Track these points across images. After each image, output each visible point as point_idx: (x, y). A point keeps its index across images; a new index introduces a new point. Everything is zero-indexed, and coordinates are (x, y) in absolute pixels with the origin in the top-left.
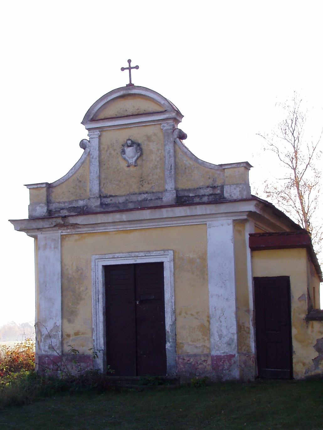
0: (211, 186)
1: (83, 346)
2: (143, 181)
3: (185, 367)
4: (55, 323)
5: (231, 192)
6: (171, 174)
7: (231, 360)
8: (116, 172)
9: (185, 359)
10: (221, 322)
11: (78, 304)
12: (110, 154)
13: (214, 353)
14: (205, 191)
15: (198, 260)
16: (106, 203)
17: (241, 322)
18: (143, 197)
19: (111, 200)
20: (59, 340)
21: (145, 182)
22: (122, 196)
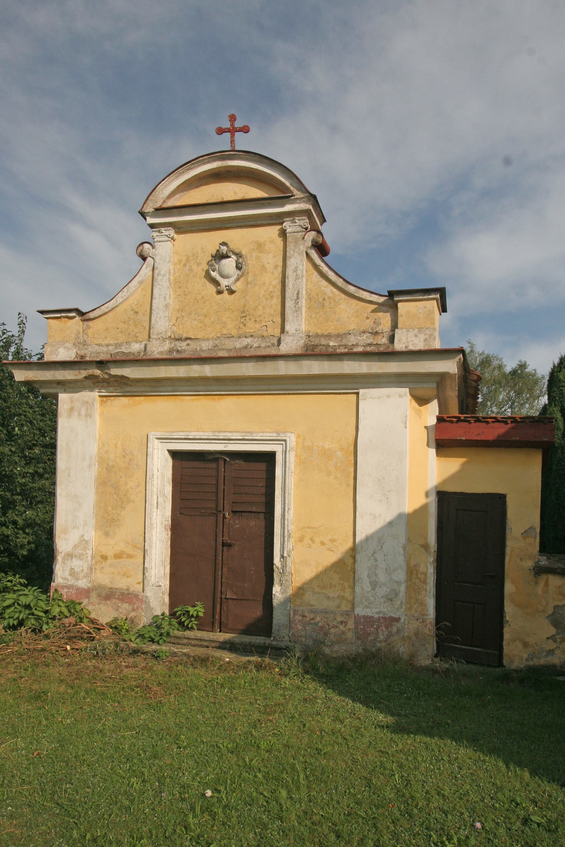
0: (370, 331)
1: (128, 577)
2: (246, 317)
3: (305, 629)
4: (83, 536)
5: (408, 342)
6: (297, 306)
7: (391, 625)
8: (200, 300)
9: (307, 615)
10: (376, 560)
11: (123, 508)
12: (191, 270)
13: (360, 611)
14: (359, 338)
15: (339, 454)
16: (179, 349)
17: (412, 563)
18: (245, 343)
19: (188, 345)
20: (88, 564)
21: (250, 319)
22: (208, 339)
